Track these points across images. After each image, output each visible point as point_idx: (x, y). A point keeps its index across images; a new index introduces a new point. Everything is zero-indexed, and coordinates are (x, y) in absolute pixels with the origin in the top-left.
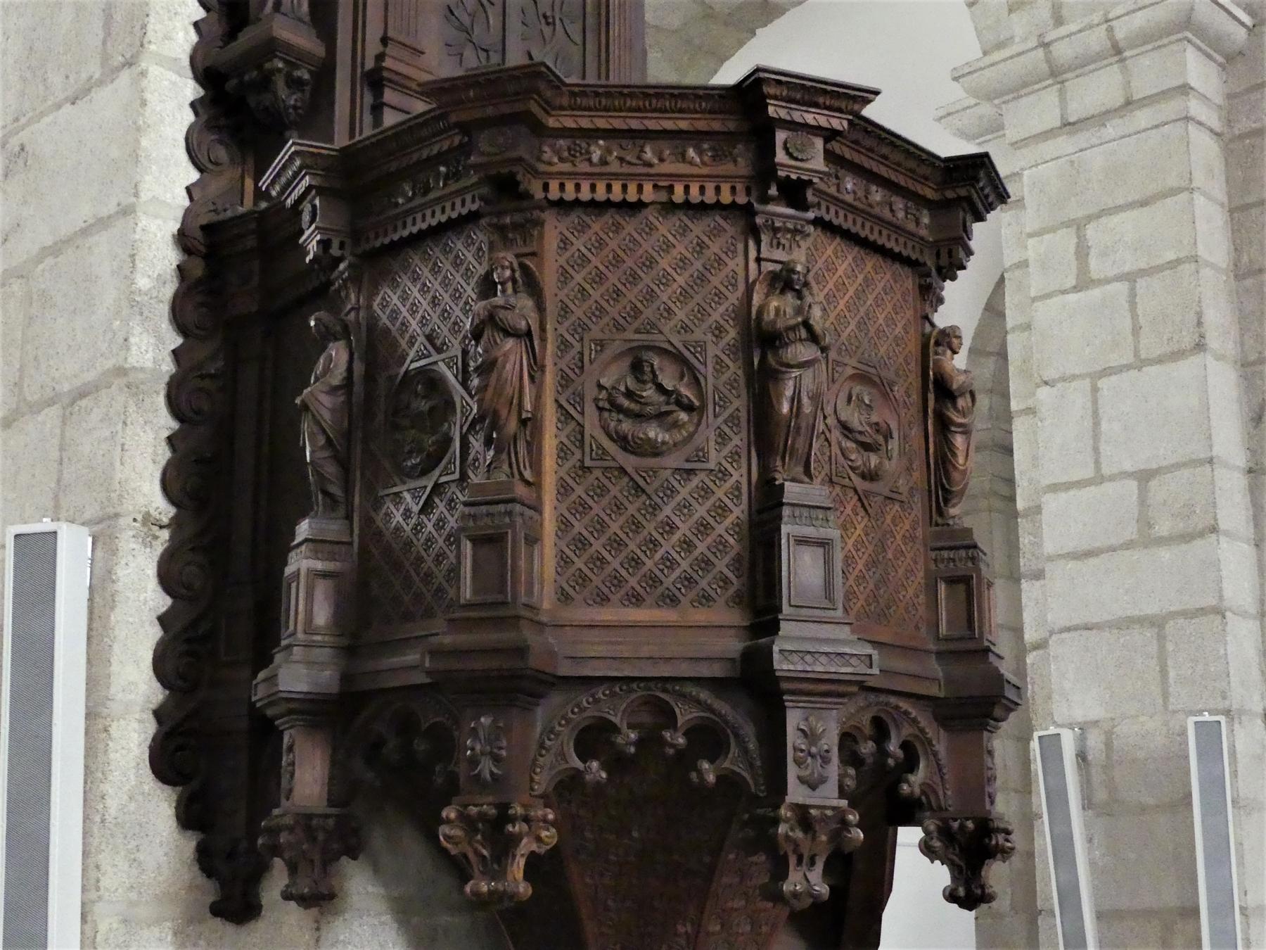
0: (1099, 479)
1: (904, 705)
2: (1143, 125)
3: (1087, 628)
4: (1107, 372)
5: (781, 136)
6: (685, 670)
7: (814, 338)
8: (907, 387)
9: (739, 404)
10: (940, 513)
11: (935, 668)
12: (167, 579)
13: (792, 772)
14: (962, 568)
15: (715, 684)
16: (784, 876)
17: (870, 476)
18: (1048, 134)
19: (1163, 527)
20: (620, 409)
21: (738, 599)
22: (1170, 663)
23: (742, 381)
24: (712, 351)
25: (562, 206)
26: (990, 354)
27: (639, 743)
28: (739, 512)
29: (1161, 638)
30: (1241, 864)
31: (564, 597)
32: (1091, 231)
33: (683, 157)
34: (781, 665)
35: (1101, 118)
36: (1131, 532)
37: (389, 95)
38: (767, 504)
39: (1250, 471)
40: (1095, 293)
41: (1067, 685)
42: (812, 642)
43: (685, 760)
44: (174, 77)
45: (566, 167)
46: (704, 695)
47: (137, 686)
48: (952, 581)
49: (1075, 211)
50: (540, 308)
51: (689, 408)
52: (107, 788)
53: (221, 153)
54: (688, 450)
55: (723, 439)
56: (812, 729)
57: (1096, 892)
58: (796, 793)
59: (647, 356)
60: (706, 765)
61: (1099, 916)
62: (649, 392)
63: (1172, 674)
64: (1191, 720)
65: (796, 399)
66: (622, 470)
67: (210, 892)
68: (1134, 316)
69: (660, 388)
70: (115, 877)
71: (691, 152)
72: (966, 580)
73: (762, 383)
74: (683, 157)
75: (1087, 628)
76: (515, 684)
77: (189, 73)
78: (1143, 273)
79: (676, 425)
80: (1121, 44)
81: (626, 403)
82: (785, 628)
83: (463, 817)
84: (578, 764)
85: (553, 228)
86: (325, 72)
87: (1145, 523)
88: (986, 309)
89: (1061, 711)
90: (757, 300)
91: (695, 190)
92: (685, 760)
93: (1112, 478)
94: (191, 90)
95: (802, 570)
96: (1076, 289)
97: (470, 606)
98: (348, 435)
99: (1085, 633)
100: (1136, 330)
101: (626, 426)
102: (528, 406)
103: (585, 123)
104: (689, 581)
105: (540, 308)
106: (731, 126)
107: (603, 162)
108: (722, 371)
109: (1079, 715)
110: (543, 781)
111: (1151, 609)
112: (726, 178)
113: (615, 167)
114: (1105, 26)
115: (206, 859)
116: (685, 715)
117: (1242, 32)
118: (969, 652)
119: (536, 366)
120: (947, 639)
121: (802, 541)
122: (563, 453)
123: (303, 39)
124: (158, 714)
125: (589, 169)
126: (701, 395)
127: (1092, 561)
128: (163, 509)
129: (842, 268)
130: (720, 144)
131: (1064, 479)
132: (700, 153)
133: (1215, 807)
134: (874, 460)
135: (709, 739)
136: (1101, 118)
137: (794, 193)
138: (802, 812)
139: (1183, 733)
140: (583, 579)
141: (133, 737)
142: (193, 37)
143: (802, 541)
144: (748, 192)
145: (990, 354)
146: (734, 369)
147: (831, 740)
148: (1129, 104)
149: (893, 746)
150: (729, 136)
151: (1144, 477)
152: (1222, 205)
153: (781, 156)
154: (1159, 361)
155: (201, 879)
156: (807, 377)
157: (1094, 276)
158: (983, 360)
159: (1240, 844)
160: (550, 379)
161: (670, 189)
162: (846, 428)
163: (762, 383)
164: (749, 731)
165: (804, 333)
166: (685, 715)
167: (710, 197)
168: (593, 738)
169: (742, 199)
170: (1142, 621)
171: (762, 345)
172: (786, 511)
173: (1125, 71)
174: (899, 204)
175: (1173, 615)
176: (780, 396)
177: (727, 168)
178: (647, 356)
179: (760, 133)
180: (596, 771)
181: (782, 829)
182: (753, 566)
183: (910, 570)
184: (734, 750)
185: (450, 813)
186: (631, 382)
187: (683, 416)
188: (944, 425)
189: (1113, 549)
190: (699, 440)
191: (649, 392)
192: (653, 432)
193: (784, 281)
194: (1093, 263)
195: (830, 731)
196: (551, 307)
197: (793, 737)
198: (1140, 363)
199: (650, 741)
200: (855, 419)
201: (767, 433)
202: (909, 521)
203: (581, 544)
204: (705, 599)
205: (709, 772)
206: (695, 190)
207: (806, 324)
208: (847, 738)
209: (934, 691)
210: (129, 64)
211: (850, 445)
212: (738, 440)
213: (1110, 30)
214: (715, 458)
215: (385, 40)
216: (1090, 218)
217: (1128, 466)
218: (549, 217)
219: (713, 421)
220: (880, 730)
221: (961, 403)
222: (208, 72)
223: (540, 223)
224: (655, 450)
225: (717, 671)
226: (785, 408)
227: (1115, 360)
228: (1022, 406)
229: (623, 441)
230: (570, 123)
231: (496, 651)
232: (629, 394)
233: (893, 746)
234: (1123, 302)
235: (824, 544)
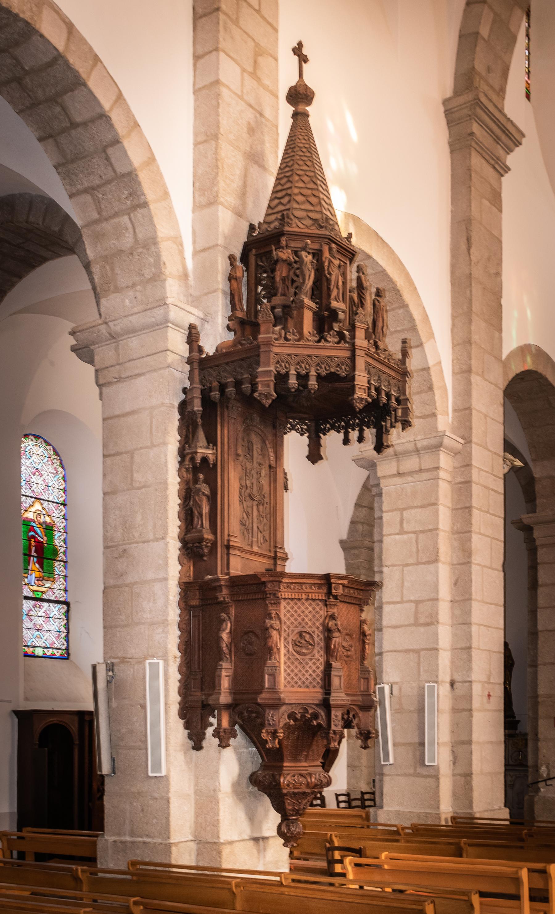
0: (401, 602)
1: (353, 707)
2: (425, 478)
3: (395, 651)
4: (407, 565)
5: (333, 585)
6: (311, 702)
7: (339, 630)
8: (356, 635)
9: (322, 644)
10: (362, 663)
11: (360, 698)
12: (180, 672)
13: (332, 723)
14: (366, 676)
15: (317, 705)
16: (330, 744)
17: (348, 656)
18: (393, 476)
19: (422, 620)
20: (297, 645)
21: (321, 687)
22: (421, 665)
23: (323, 640)
24: (317, 632)
25: (285, 599)
26: (364, 507)
27: (301, 717)
28: (322, 668)
29: (419, 657)
30: (438, 729)
31: (285, 686)
32: (405, 513)
33: (311, 588)
34: (332, 703)
35: (411, 473)
36: (412, 621)
37: (231, 551)
38: (328, 667)
39: (452, 601)
40: (405, 536)
41: (388, 670)
42: (339, 697)
43: (310, 720)
44: (174, 542)
45: (286, 590)
46: (314, 707)
47: (175, 698)
48: (364, 678)
49: (400, 505)
50: (281, 623)
51: (311, 645)
52: (170, 721)
53: (185, 561)
54: (311, 654)
55: (319, 652)
56: (337, 715)
57: (394, 737)
58: (333, 728)
59: (304, 634)
60: (314, 721)
61: (395, 745)
62: (303, 641)
63: (422, 668)
64: (427, 684)
65: (335, 645)
66: (297, 659)
67: (191, 743)
68: (417, 547)
69: (306, 641)
70: (172, 741)
71: (313, 587)
72: (367, 679)
73: (328, 640)
74: (311, 588)
75: (395, 651)
76: (277, 704)
77: (178, 540)
78: (422, 532)
79: (309, 649)
80: (419, 449)
81: (298, 644)
82: (333, 694)
83: (267, 731)
84: (288, 721)
85: (283, 603)
86: (215, 543)
87: (416, 618)
88: (363, 487)
89: (385, 678)
90: (327, 621)
91: (314, 596)
92: (310, 720)
93: (407, 602)
94: (179, 545)
95: (335, 681)
96: (398, 534)
97: (268, 688)
98: (231, 644)
99: (395, 653)
100: (418, 551)
101: (298, 649)
102: (279, 645)
103: (291, 581)
104: (311, 683)
105: (281, 623)
106: (322, 582)
107: (294, 589)
108: (318, 637)
109: (392, 680)
110: (281, 724)
111: (416, 647)
112: (320, 593)
113: (296, 590)
114: (414, 442)
115: (190, 737)
116: (310, 711)
117: (460, 446)
118: (367, 695)
119: (280, 635)
120: (363, 691)
121: (336, 676)
122: (285, 655)
123: (208, 536)
124: (180, 704)
125: (291, 591)
126: (314, 643)
127: (399, 629)
128: (179, 654)
129: (344, 609)
130: (320, 586)
131: (391, 600)
132: (315, 587)
133: (432, 712)
134: (349, 653)
135: (315, 716)
136: (411, 473)
137: (336, 597)
138: (334, 731)
139: (424, 688)
140: (289, 682)
141: (175, 708)
142: (178, 530)
143: (336, 676)
144: (325, 596)
145: (364, 507)
146: (321, 636)
147: (340, 717)
148: (420, 471)
149: (351, 716)
150: (322, 584)
151: (417, 602)
152: (449, 508)
153: (333, 591)
154: (423, 563)
155: (187, 740)
156: (337, 640)
157: (405, 530)
158: (360, 509)
159: (438, 723)
160: (282, 639)
161: (308, 596)
162: (344, 647)
163: (328, 640)
164: (323, 714)
165: (337, 630)
166: (310, 711)
167: (317, 598)
168: (291, 716)
169: (324, 598)
170: (413, 651)
171: (328, 632)
172: (333, 669)
173: (419, 457)
174: (356, 591)
175: (423, 650)
176: (331, 644)
177: (320, 591)
178: (304, 634)
179: (329, 585)
180: (292, 722)
181: (331, 735)
182: (325, 679)
183: (355, 675)
184: (320, 718)
185: (264, 731)
186: (299, 639)
187: (310, 647)
188: (364, 643)
189: (406, 626)
190: (314, 652)
191: (303, 641)
192: (304, 651)
193: (332, 617)
194: (405, 525)
195: (339, 714)
196: (283, 622)
197: (333, 717)
198: (418, 563)
199: (303, 716)
200: (345, 644)
201: (328, 651)
202: (355, 665)
203: (289, 675)
204: (314, 687)
205: (315, 723)
206: (314, 596)
207: (338, 628)
208: (343, 715)
209: (360, 704)
210: (163, 538)
211: (344, 650)
212: (322, 653)
213: (415, 444)
214: (317, 656)
215: (229, 535)
216: (405, 509)
217: (412, 598)
218: (282, 601)
219: (317, 648)
220: (348, 713)
221: (368, 637)
222: (183, 540)
223: (279, 603)
224: (304, 654)
225: (317, 702)
226: (332, 647)
227: (411, 561)
228: (378, 570)
229: (298, 653)
230: (287, 581)
231: (272, 699)
232: (299, 642)
233: (351, 716)
234: (414, 541)
235: (340, 676)
